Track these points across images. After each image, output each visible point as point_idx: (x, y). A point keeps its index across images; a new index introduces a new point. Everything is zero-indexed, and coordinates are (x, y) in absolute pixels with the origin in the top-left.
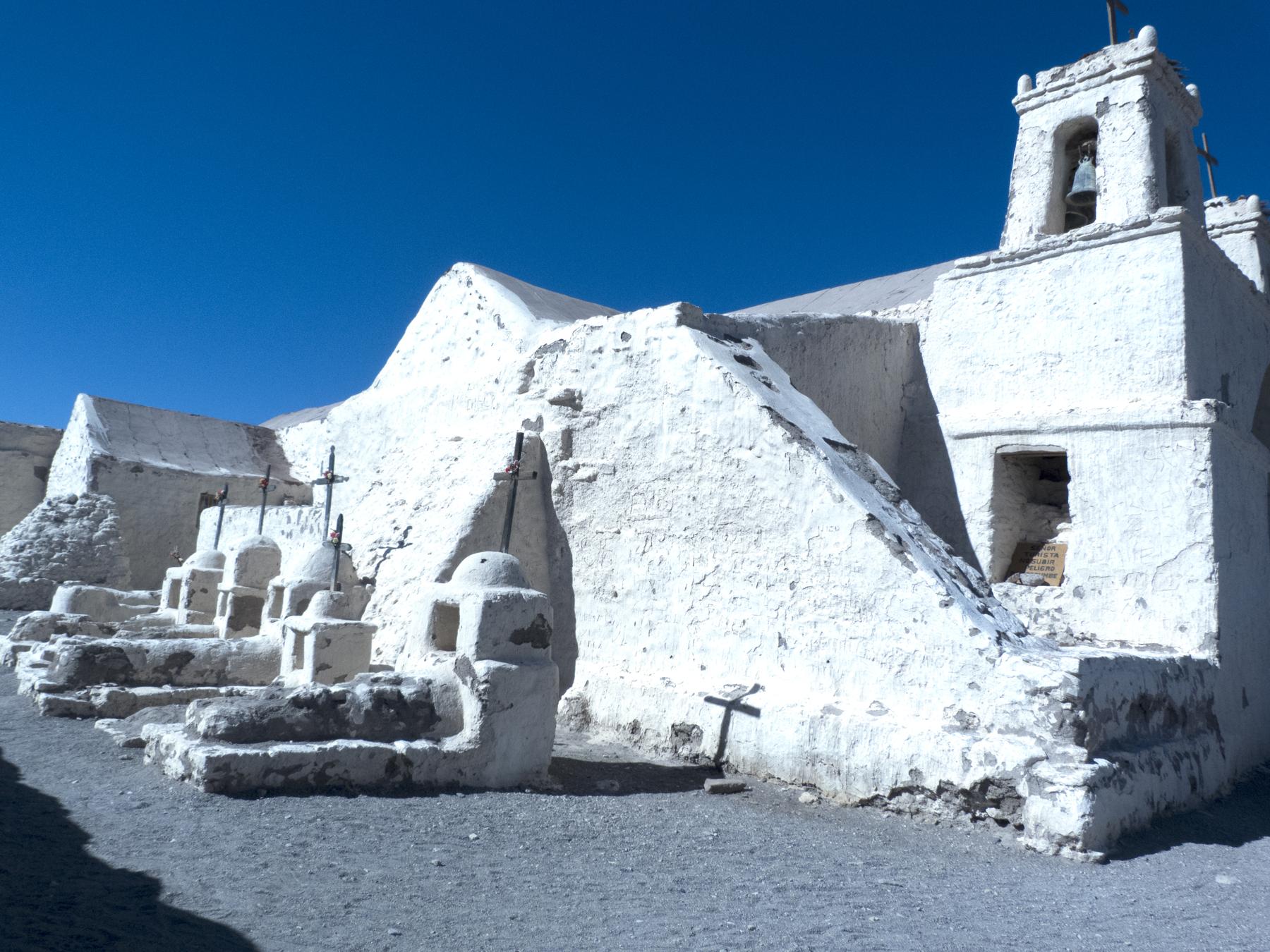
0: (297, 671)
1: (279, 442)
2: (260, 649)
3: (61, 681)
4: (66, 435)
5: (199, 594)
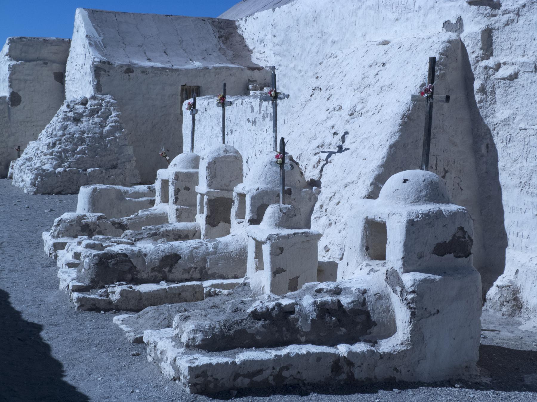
0: (260, 272)
1: (239, 31)
2: (231, 248)
3: (87, 282)
4: (72, 44)
5: (183, 192)
